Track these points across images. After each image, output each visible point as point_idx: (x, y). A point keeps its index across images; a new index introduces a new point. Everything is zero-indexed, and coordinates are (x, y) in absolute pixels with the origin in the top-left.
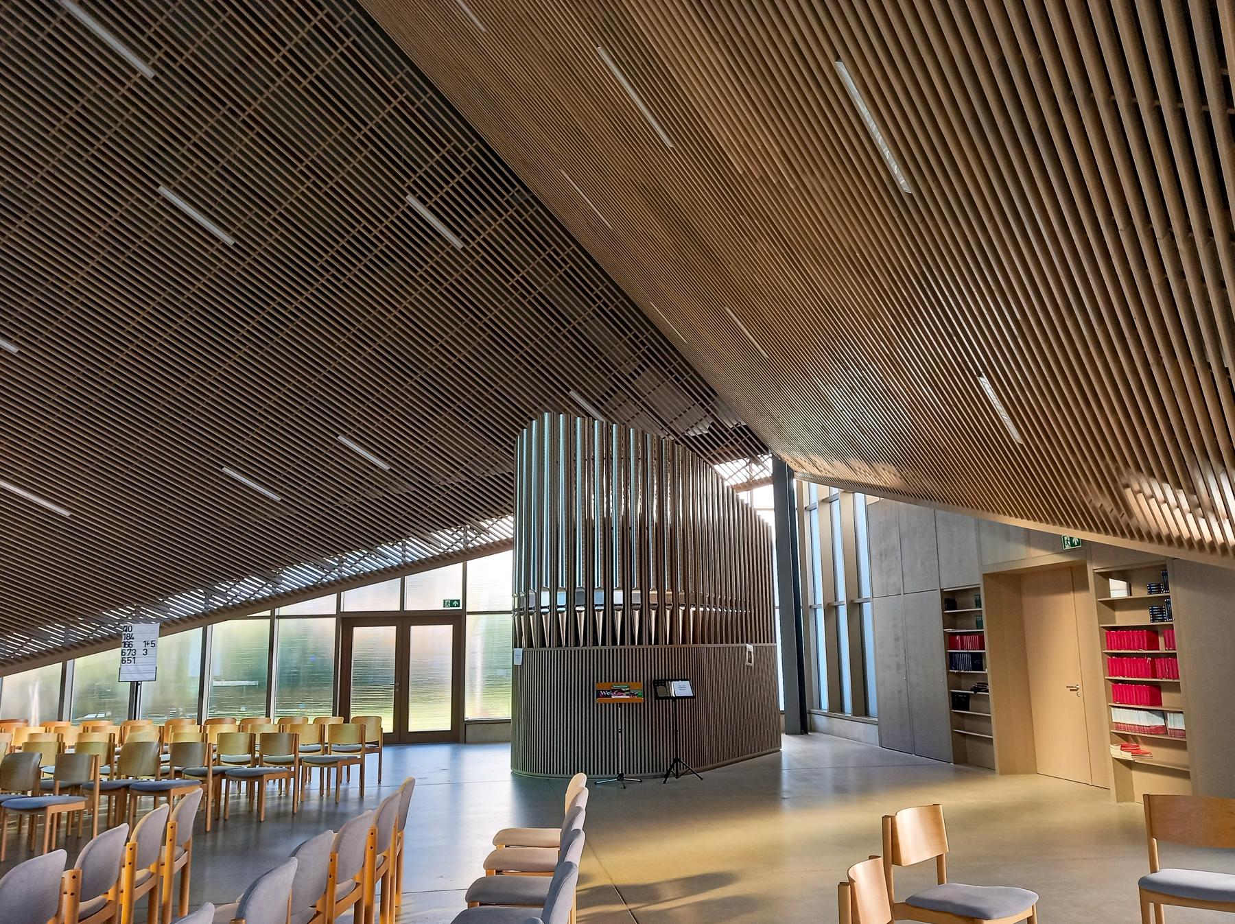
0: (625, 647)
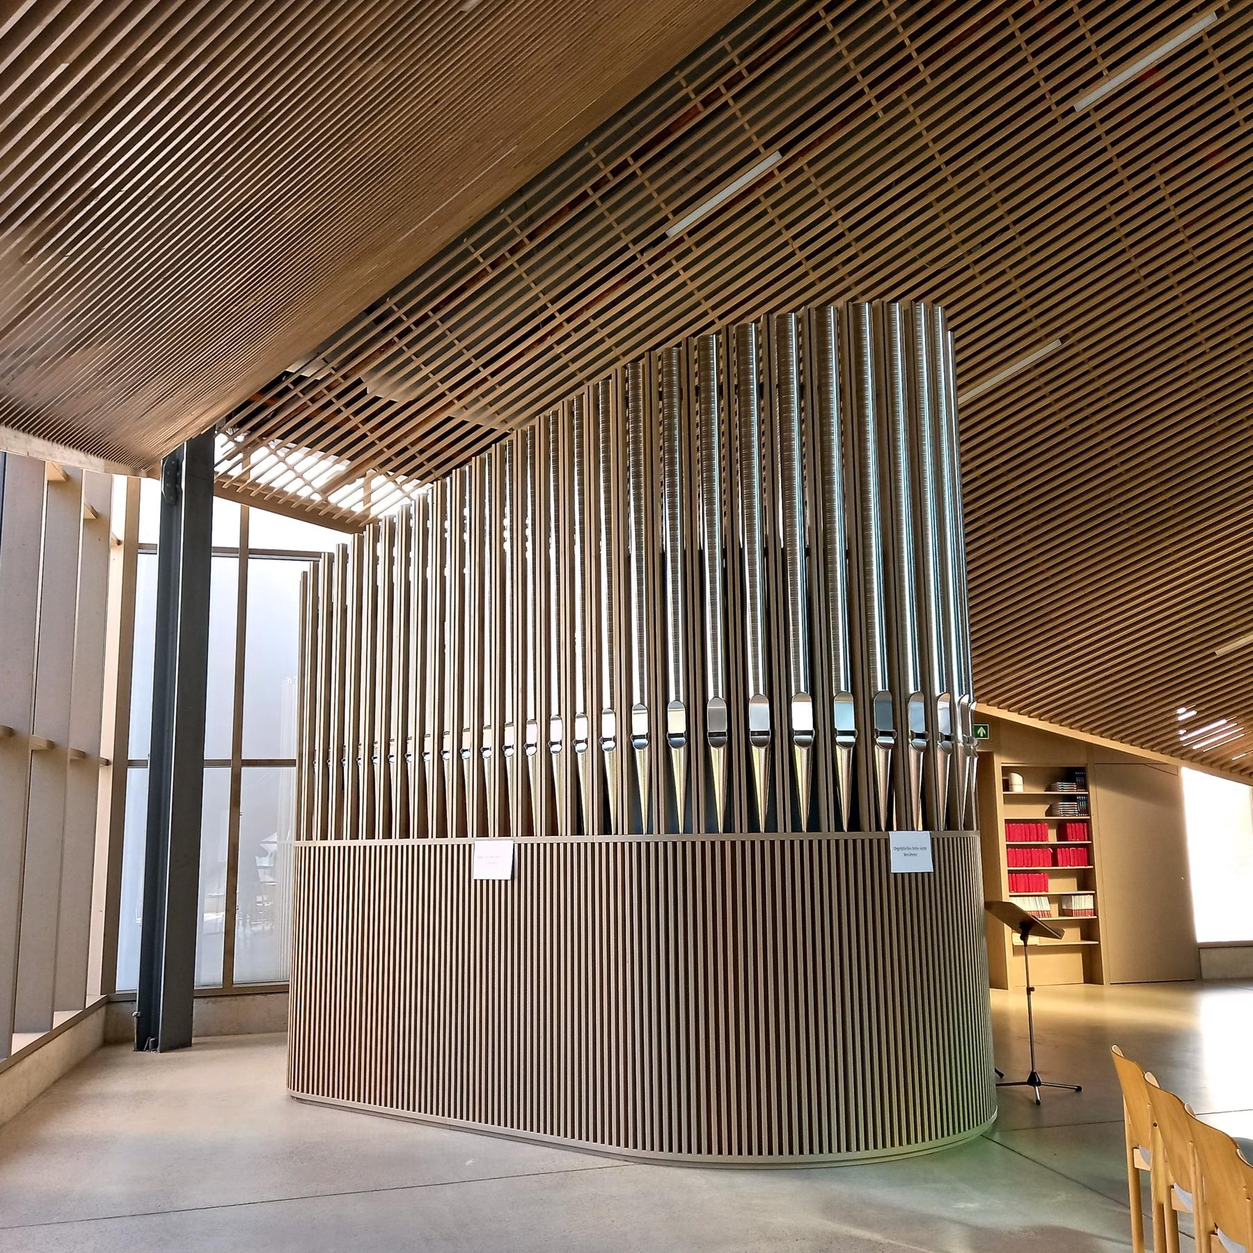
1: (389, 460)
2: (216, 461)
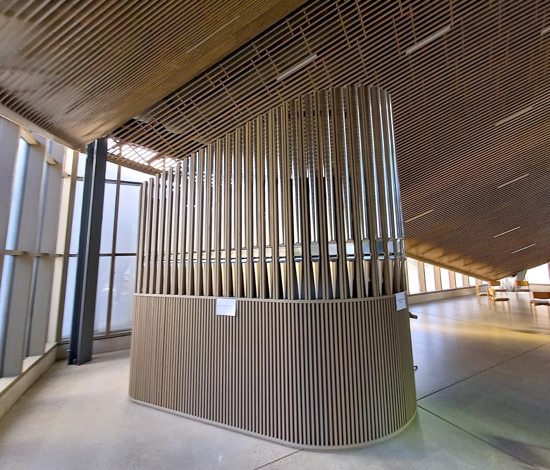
1: (173, 152)
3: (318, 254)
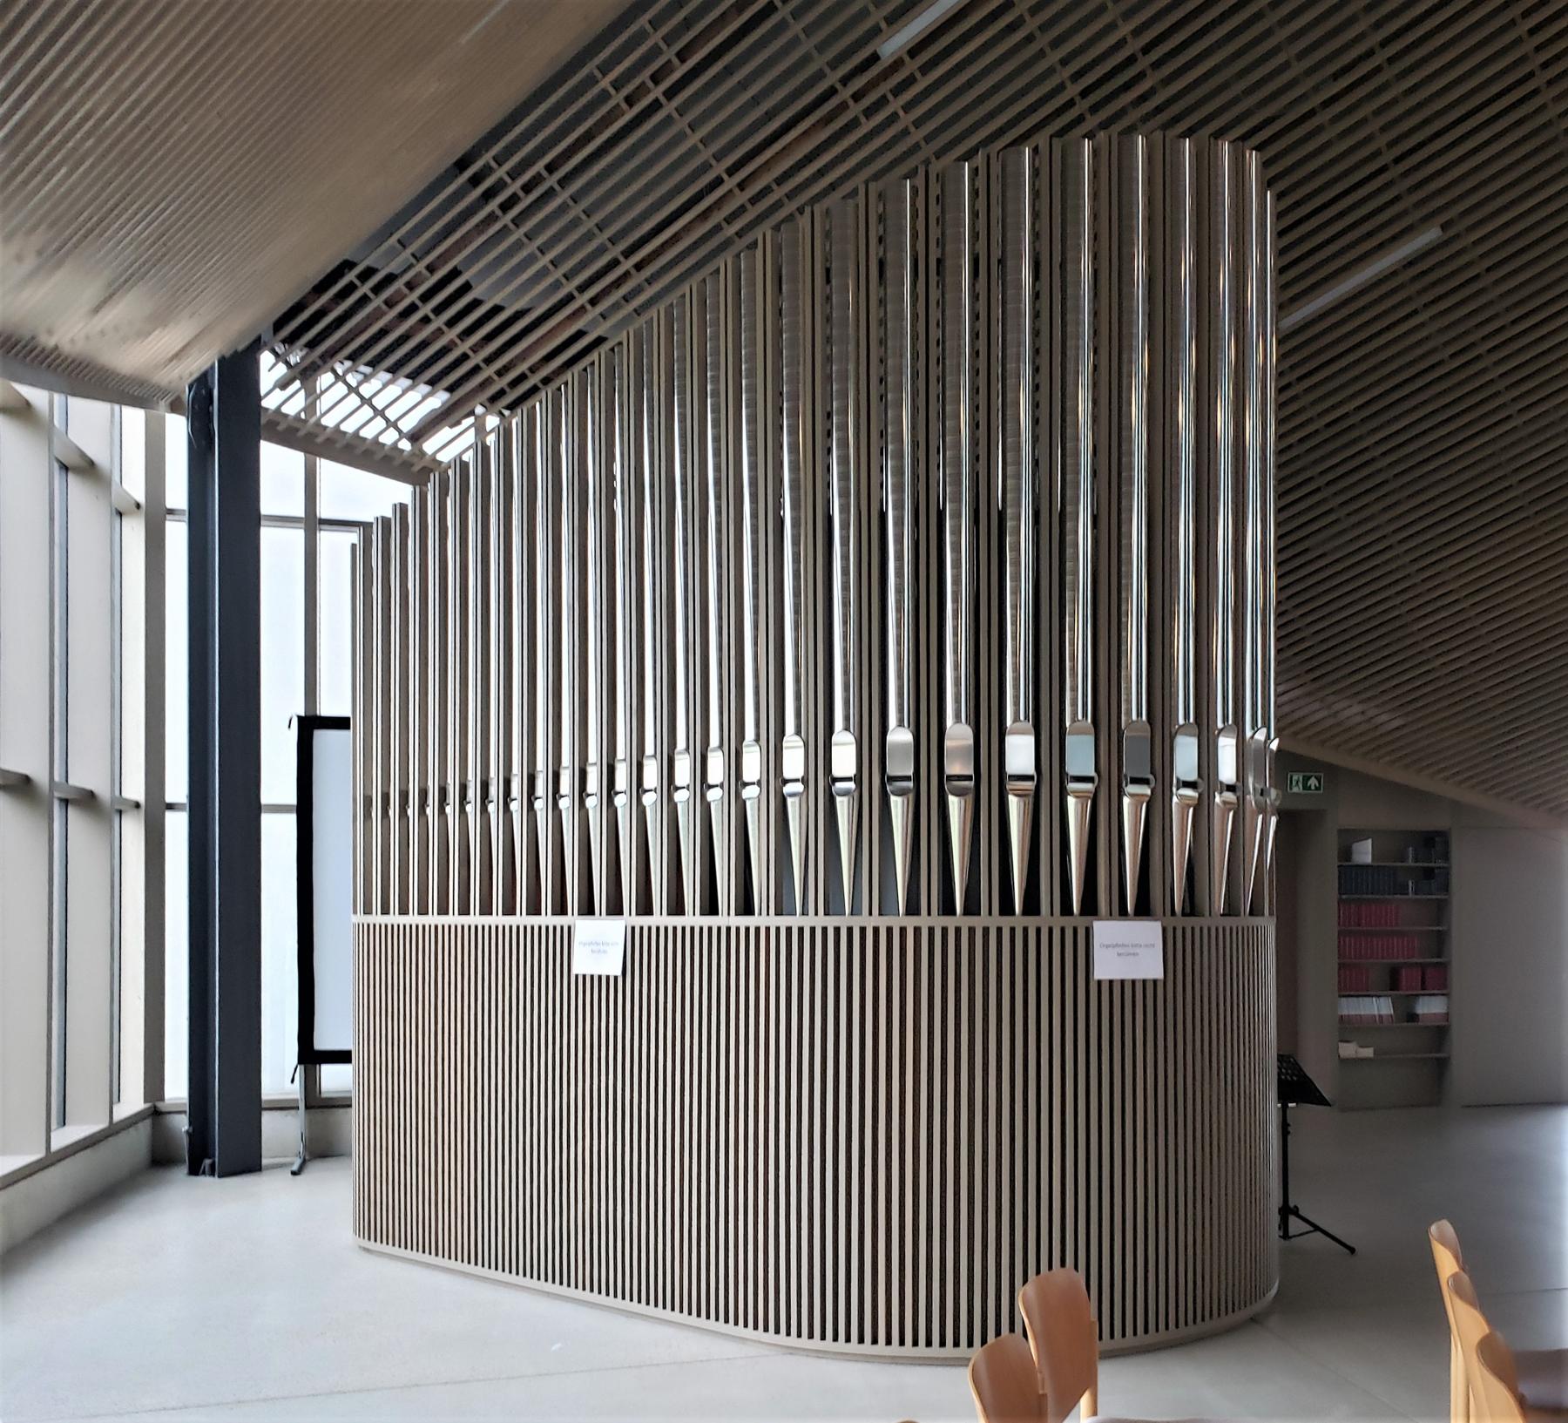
0: (978, 922)
2: (263, 393)
3: (910, 772)
